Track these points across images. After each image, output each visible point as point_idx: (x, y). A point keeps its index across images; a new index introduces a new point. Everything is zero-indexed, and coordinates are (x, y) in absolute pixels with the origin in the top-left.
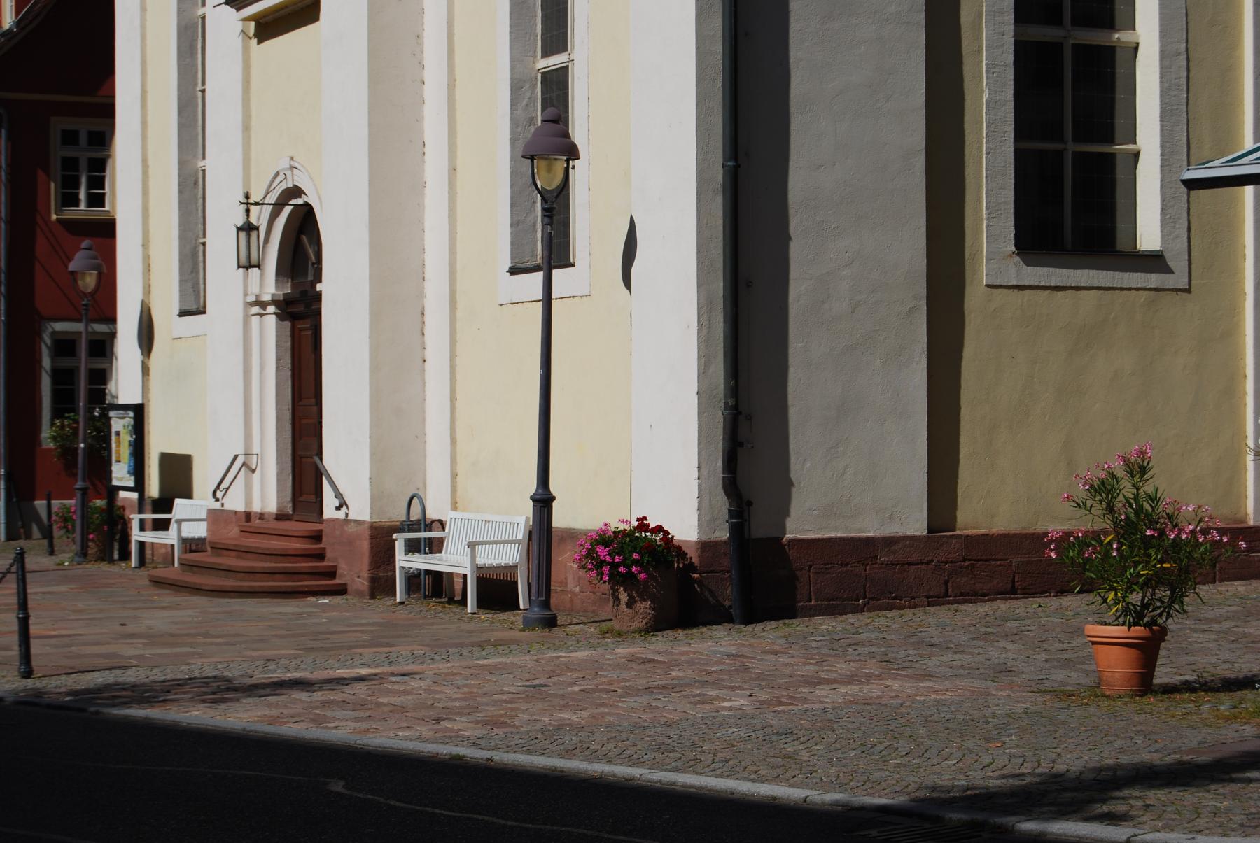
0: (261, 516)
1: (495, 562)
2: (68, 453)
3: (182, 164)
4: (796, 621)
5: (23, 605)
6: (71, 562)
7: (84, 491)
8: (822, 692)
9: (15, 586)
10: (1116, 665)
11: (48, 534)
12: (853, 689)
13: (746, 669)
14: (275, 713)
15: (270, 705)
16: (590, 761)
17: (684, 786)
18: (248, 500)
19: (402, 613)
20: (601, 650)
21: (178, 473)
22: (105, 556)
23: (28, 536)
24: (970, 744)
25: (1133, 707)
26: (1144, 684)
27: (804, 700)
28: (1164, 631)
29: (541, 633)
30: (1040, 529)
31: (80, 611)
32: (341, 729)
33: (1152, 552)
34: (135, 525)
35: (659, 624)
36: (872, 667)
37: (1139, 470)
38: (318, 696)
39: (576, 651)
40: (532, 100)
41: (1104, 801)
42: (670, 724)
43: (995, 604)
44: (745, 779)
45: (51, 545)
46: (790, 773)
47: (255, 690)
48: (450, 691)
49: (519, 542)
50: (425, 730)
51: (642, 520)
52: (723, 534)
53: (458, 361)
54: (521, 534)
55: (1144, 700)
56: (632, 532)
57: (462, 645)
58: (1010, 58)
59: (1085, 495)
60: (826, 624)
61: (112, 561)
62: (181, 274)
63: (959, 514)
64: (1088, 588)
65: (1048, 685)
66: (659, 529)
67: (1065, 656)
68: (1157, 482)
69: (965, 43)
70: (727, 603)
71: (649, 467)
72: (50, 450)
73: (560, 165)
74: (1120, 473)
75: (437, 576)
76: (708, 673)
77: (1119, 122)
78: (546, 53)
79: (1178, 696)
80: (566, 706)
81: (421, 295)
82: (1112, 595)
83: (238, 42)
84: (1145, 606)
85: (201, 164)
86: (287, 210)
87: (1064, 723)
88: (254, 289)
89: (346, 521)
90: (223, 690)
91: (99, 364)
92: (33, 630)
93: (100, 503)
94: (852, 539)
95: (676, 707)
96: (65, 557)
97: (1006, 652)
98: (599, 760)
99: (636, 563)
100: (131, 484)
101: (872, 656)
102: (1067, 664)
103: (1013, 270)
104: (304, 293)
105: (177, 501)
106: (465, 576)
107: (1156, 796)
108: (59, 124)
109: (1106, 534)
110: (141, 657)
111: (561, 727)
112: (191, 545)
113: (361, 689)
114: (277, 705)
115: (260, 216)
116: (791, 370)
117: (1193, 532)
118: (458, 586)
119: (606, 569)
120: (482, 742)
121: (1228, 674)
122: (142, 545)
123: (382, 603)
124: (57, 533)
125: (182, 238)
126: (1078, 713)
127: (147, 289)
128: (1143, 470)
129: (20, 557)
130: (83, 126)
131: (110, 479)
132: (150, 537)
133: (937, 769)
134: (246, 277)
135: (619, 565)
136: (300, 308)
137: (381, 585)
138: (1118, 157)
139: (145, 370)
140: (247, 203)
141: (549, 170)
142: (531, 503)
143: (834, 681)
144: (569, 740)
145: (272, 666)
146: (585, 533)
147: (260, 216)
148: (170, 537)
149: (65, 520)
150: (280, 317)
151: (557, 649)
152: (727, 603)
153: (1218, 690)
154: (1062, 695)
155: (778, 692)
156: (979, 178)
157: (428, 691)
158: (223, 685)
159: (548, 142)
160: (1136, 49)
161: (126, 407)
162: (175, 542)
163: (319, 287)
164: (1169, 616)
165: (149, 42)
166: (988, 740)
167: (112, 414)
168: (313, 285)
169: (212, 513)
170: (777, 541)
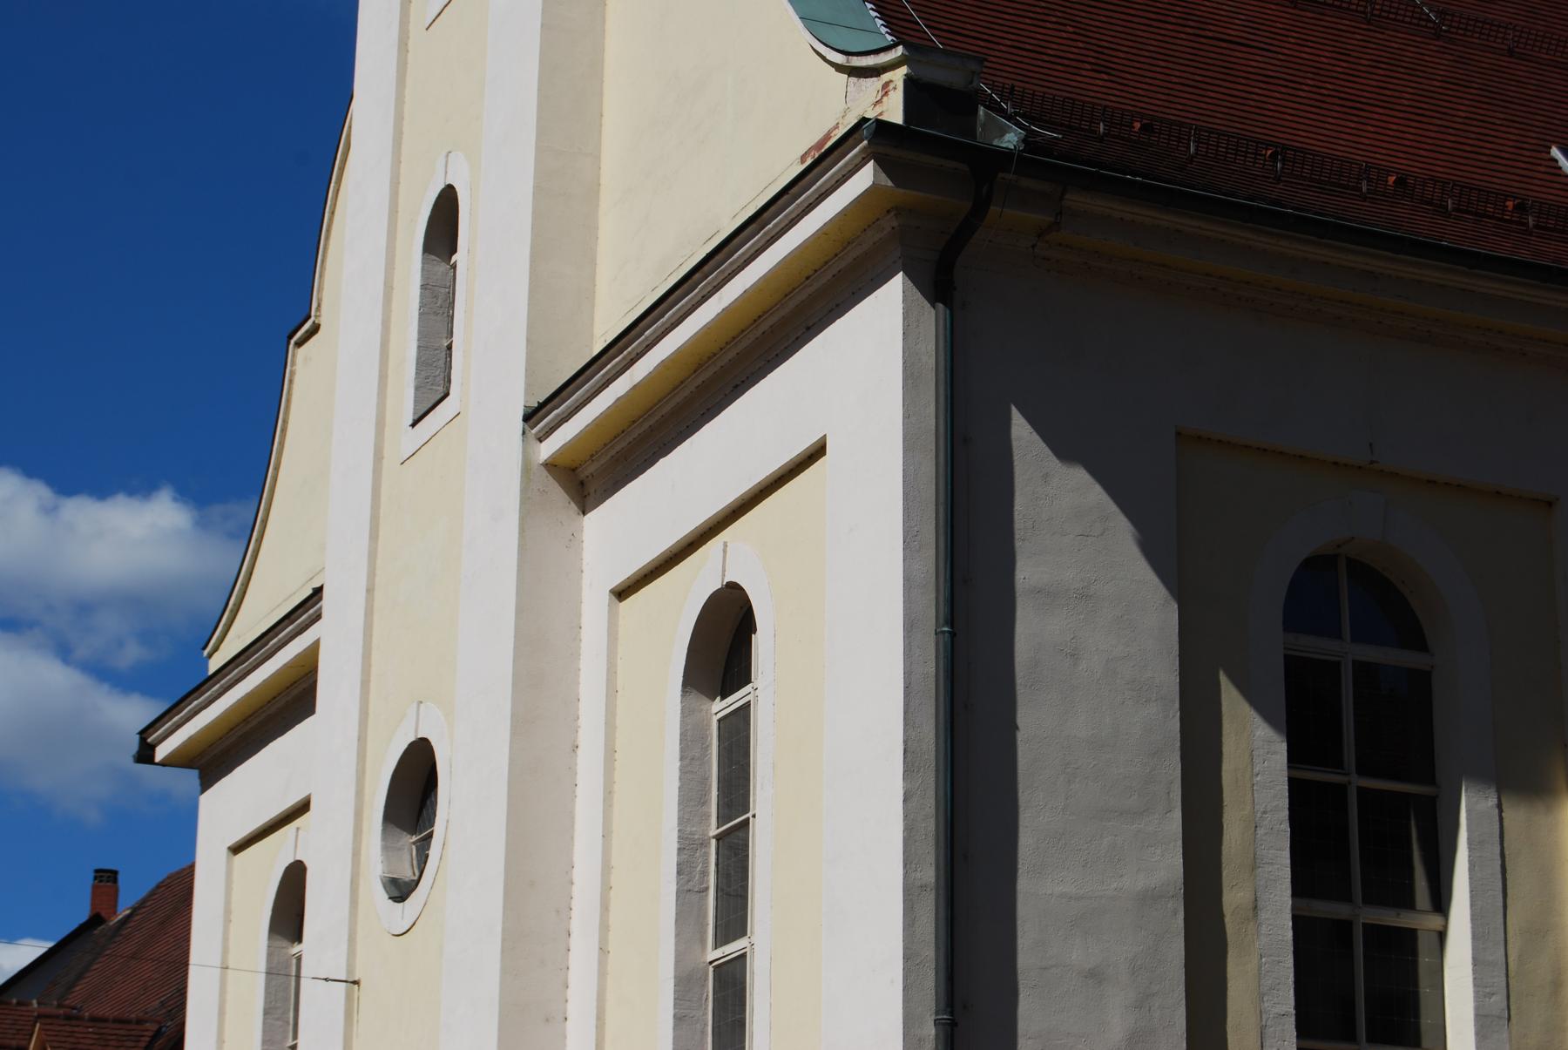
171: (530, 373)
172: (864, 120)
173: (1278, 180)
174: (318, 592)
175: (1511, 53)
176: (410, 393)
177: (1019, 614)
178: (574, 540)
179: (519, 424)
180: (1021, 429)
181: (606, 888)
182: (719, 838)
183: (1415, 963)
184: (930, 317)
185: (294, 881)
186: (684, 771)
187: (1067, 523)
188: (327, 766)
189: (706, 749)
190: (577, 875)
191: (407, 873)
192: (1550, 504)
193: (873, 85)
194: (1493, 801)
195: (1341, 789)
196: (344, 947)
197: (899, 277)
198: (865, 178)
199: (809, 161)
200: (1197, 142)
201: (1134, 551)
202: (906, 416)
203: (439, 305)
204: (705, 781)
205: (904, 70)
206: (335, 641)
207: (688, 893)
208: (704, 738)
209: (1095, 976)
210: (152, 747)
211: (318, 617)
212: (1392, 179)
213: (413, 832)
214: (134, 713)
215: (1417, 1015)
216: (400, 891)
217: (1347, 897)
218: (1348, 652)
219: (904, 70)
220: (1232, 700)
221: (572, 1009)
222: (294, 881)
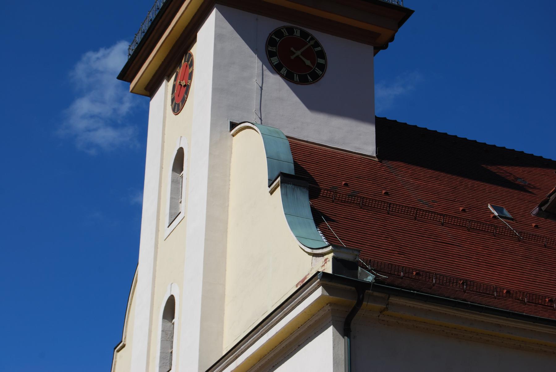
172: (318, 272)
184: (342, 341)
193: (322, 259)
198: (319, 292)
199: (299, 287)
212: (505, 291)
219: (332, 254)
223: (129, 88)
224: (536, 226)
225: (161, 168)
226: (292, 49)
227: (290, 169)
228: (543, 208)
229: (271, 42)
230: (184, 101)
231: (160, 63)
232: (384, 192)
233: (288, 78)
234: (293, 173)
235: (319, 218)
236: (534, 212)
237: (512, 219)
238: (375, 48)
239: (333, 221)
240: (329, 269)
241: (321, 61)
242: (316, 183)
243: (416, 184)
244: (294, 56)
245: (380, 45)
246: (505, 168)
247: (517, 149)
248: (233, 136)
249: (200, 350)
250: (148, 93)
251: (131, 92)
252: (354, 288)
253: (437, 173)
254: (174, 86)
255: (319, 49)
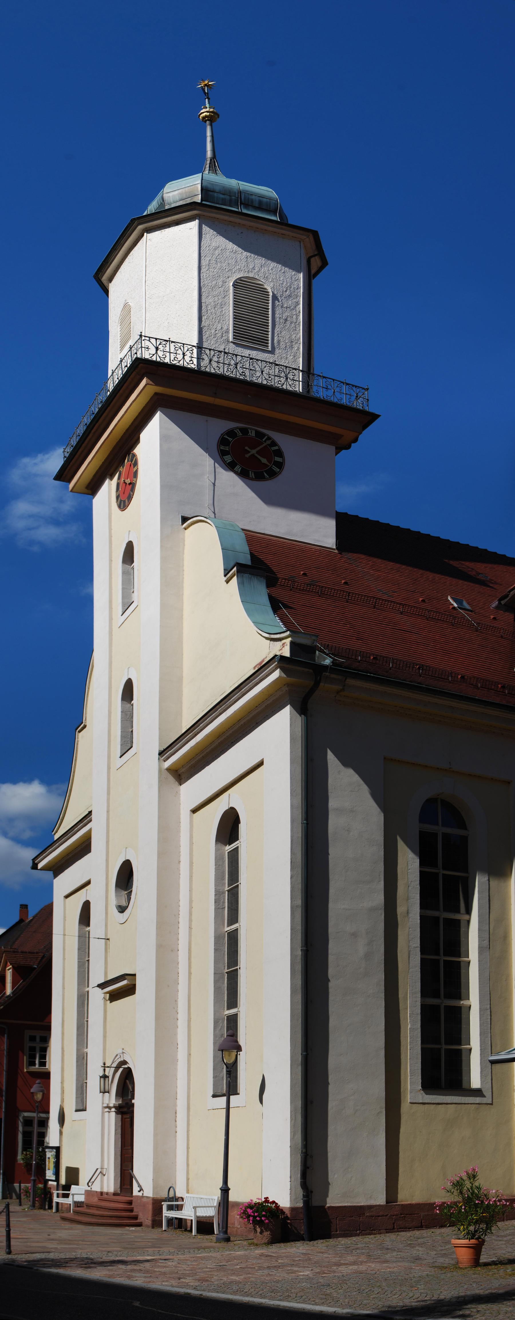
0: (107, 1194)
1: (204, 1215)
2: (28, 1165)
3: (78, 1050)
4: (331, 1240)
5: (8, 1225)
6: (28, 1208)
7: (34, 1181)
8: (342, 1268)
9: (5, 1217)
10: (464, 1255)
11: (19, 1197)
12: (355, 1267)
13: (310, 1259)
14: (111, 1273)
15: (109, 1270)
16: (243, 1296)
17: (284, 1306)
18: (102, 1187)
19: (165, 1234)
20: (248, 1251)
21: (73, 1175)
22: (42, 1207)
23: (11, 1198)
24: (404, 1289)
25: (471, 1272)
26: (476, 1262)
27: (334, 1272)
28: (484, 1241)
29: (224, 1244)
30: (432, 1201)
31: (31, 1229)
32: (139, 1281)
33: (478, 1209)
34: (55, 1195)
35: (273, 1241)
36: (363, 1258)
37: (473, 1176)
38: (129, 1267)
39: (238, 1252)
40: (223, 1027)
41: (460, 1310)
42: (278, 1282)
43: (414, 1232)
44: (309, 1304)
45: (20, 1202)
46: (328, 1301)
47: (103, 1264)
48: (185, 1267)
49: (215, 1207)
50: (174, 1282)
51: (266, 1198)
52: (300, 1204)
53: (190, 1132)
54: (215, 1204)
55: (476, 1269)
56: (262, 1203)
57: (190, 1248)
58: (419, 1011)
59: (451, 1187)
60: (343, 1241)
61: (45, 1209)
62: (77, 1094)
63: (399, 1196)
64: (452, 1225)
65: (436, 1264)
66: (274, 1202)
67: (443, 1252)
68: (481, 1181)
69: (401, 1005)
70: (302, 1232)
71: (271, 1179)
72: (21, 1164)
73: (234, 1054)
74: (465, 1178)
75: (180, 1220)
76: (294, 1261)
77: (463, 1036)
78: (229, 1008)
79: (490, 1267)
80: (234, 1274)
81: (175, 1105)
82: (462, 1227)
83: (102, 1002)
84: (476, 1231)
85: (86, 1050)
86: (121, 1070)
87: (443, 1279)
88: (106, 1101)
89: (143, 1197)
90: (89, 1263)
91: (42, 1130)
92: (12, 1235)
93: (41, 1186)
94: (355, 1206)
95: (280, 1275)
96: (26, 1207)
97: (419, 1251)
98: (247, 1296)
99: (264, 1216)
100: (54, 1179)
101: (363, 1254)
102: (444, 1255)
103: (421, 1096)
104: (127, 1104)
105: (73, 1186)
106: (192, 1220)
107: (482, 1307)
108: (28, 1033)
109: (460, 1203)
110: (56, 1248)
111: (231, 1282)
112: (78, 1204)
113: (147, 1265)
114: (112, 1270)
115: (110, 1072)
116: (329, 1138)
117: (495, 1201)
118: (189, 1224)
119: (251, 1218)
120: (198, 1288)
121: (510, 1257)
122: (57, 1203)
123: (157, 1230)
124: (23, 1197)
125: (77, 1080)
126: (449, 1275)
127: (62, 1100)
128: (474, 1177)
129: (8, 1206)
130: (38, 1034)
131: (45, 1176)
132: (61, 1200)
133: (390, 1299)
134: (103, 1097)
135: (256, 1217)
136: (125, 1110)
137: (156, 1223)
138: (463, 1051)
139: (61, 1133)
140: (104, 1066)
141: (229, 1055)
142: (220, 1191)
143: (347, 1264)
144: (235, 1287)
145: (110, 1254)
146: (242, 1204)
147: (110, 1072)
148: (69, 1201)
149: (26, 1192)
150: (117, 1113)
151: (230, 1251)
152: (302, 1232)
153: (506, 1264)
154: (442, 1268)
155: (323, 1269)
156: (407, 1059)
157: (176, 1267)
158: (90, 1261)
159: (229, 1044)
160: (470, 1007)
161: (52, 1148)
162: (71, 1203)
163: (133, 1101)
164: (486, 1235)
165: (66, 1001)
166: (412, 1287)
167: (47, 1150)
168: (131, 1101)
169: (86, 1191)
170: (323, 1207)
171: (160, 739)
172: (276, 655)
173: (420, 676)
174: (90, 812)
175: (502, 637)
176: (119, 747)
177: (330, 817)
178: (177, 794)
179: (157, 756)
180: (330, 756)
181: (191, 908)
182: (228, 891)
183: (459, 931)
184: (299, 719)
185: (86, 907)
186: (216, 869)
187: (346, 788)
188: (96, 869)
189: (224, 862)
190: (181, 903)
191: (124, 903)
192: (509, 783)
193: (279, 644)
194: (486, 878)
195: (437, 875)
196: (104, 927)
197: (288, 707)
198: (276, 674)
199: (257, 669)
200: (393, 663)
201: (369, 796)
202: (291, 752)
203: (128, 718)
204: (224, 872)
205: (290, 639)
206: (97, 827)
207: (217, 990)
208: (223, 858)
209: (354, 935)
210: (37, 864)
211: (91, 821)
212: (459, 676)
213: (126, 890)
214: (29, 854)
215: (459, 947)
216: (122, 909)
217: (437, 909)
218: (441, 830)
219: (290, 639)
220: (401, 845)
221: (180, 947)
222: (86, 907)
223: (68, 488)
224: (494, 618)
225: (111, 560)
226: (247, 448)
227: (246, 559)
228: (503, 602)
229: (223, 441)
230: (130, 498)
231: (101, 463)
232: (343, 581)
233: (243, 475)
234: (249, 563)
235: (276, 605)
236: (494, 605)
237: (471, 611)
238: (337, 448)
239: (291, 608)
240: (286, 652)
241: (278, 459)
242: (273, 573)
243: (375, 575)
244: (249, 454)
245: (342, 445)
246: (467, 564)
247: (481, 546)
248: (185, 529)
249: (159, 729)
250: (90, 492)
251: (71, 491)
252: (311, 671)
253: (398, 565)
254: (118, 485)
255: (276, 448)
